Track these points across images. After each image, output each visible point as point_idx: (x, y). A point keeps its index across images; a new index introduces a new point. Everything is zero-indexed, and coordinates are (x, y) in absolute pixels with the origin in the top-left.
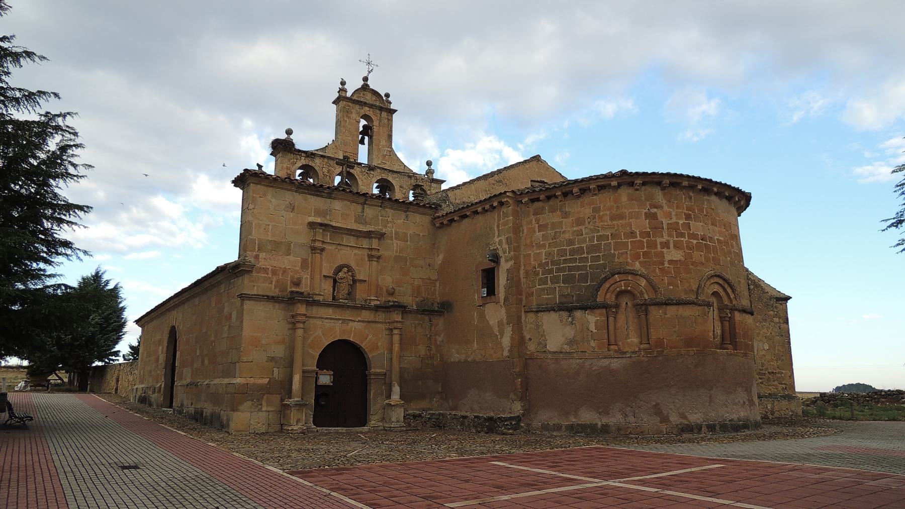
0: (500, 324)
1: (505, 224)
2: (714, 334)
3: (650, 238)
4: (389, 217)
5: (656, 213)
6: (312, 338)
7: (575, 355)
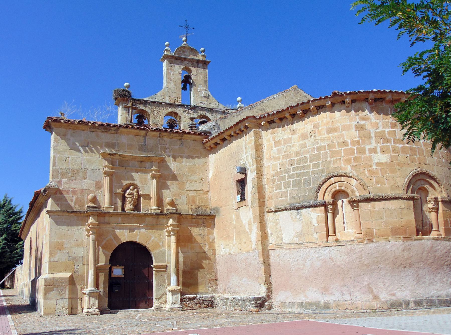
0: (249, 223)
2: (422, 223)
3: (360, 145)
4: (167, 144)
6: (105, 241)
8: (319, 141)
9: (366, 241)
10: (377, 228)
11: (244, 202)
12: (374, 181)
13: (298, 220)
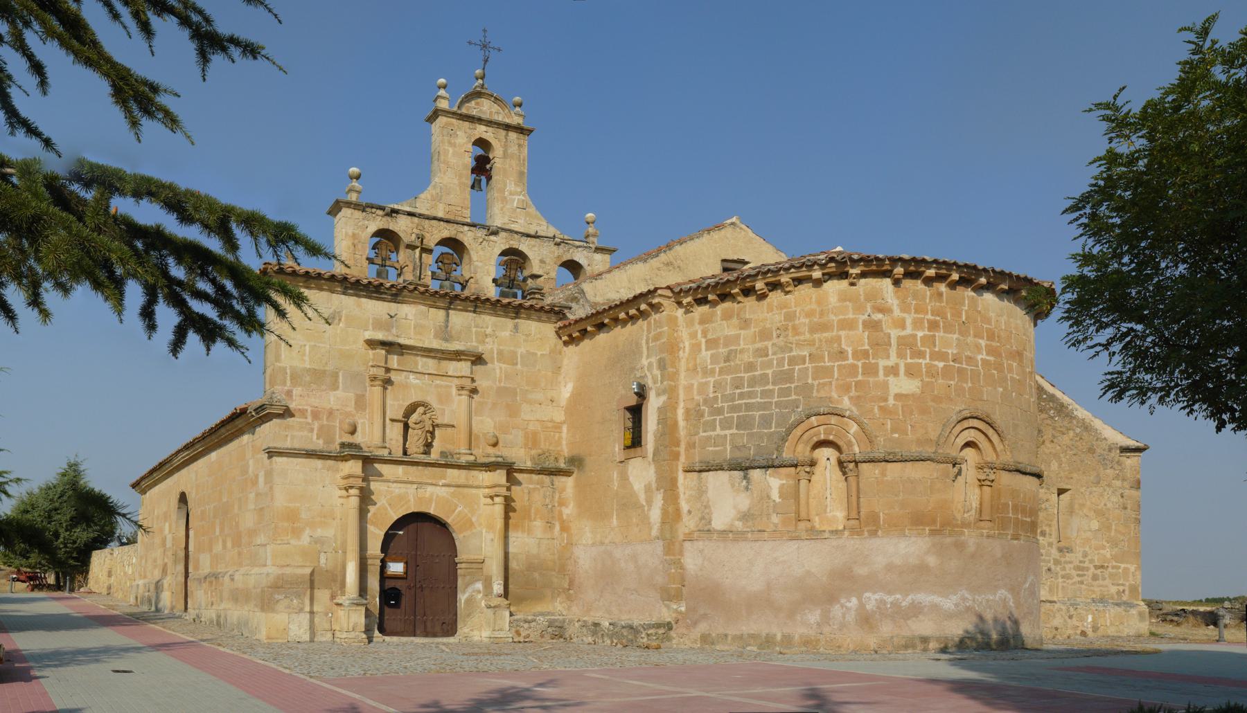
0: (648, 489)
1: (656, 338)
4: (487, 328)
5: (880, 321)
7: (749, 535)
8: (794, 346)
9: (866, 533)
10: (886, 512)
11: (639, 449)
12: (889, 426)
13: (742, 489)
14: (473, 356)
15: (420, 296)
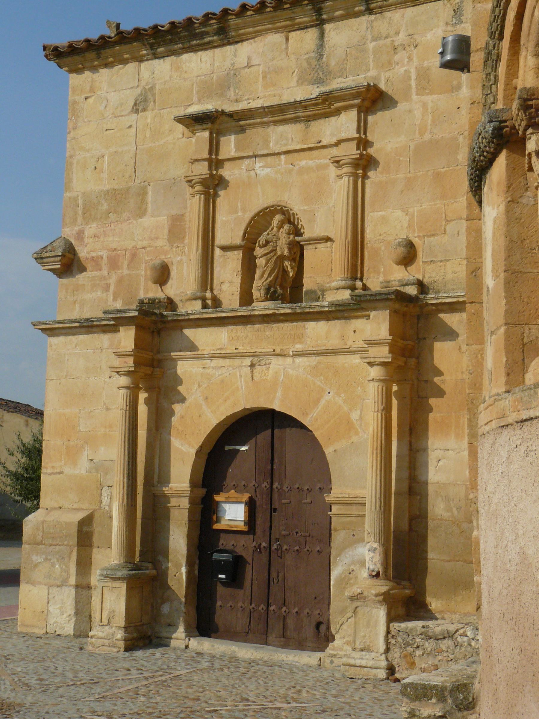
4: (397, 33)
14: (355, 96)
15: (257, 17)
